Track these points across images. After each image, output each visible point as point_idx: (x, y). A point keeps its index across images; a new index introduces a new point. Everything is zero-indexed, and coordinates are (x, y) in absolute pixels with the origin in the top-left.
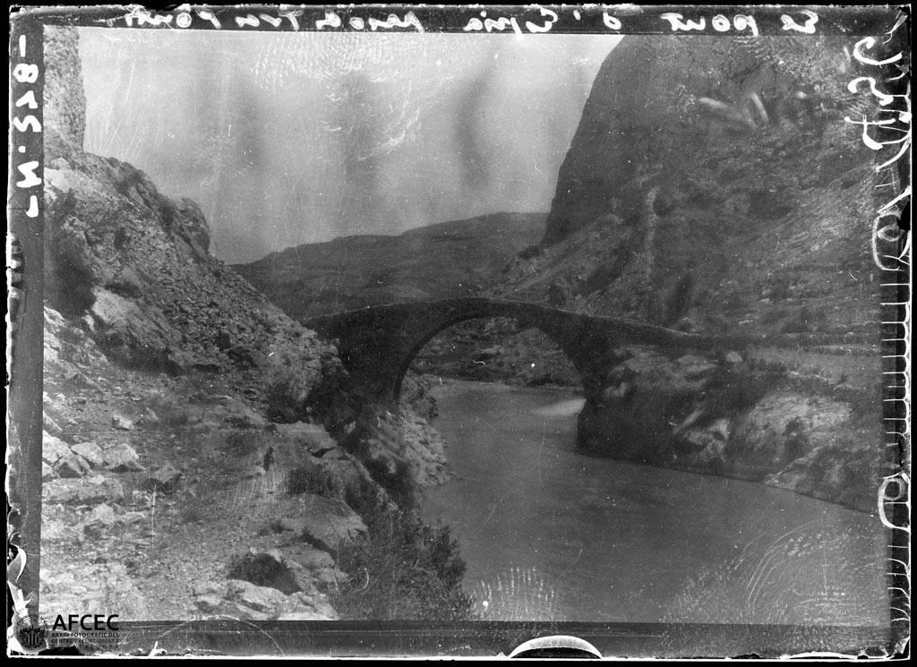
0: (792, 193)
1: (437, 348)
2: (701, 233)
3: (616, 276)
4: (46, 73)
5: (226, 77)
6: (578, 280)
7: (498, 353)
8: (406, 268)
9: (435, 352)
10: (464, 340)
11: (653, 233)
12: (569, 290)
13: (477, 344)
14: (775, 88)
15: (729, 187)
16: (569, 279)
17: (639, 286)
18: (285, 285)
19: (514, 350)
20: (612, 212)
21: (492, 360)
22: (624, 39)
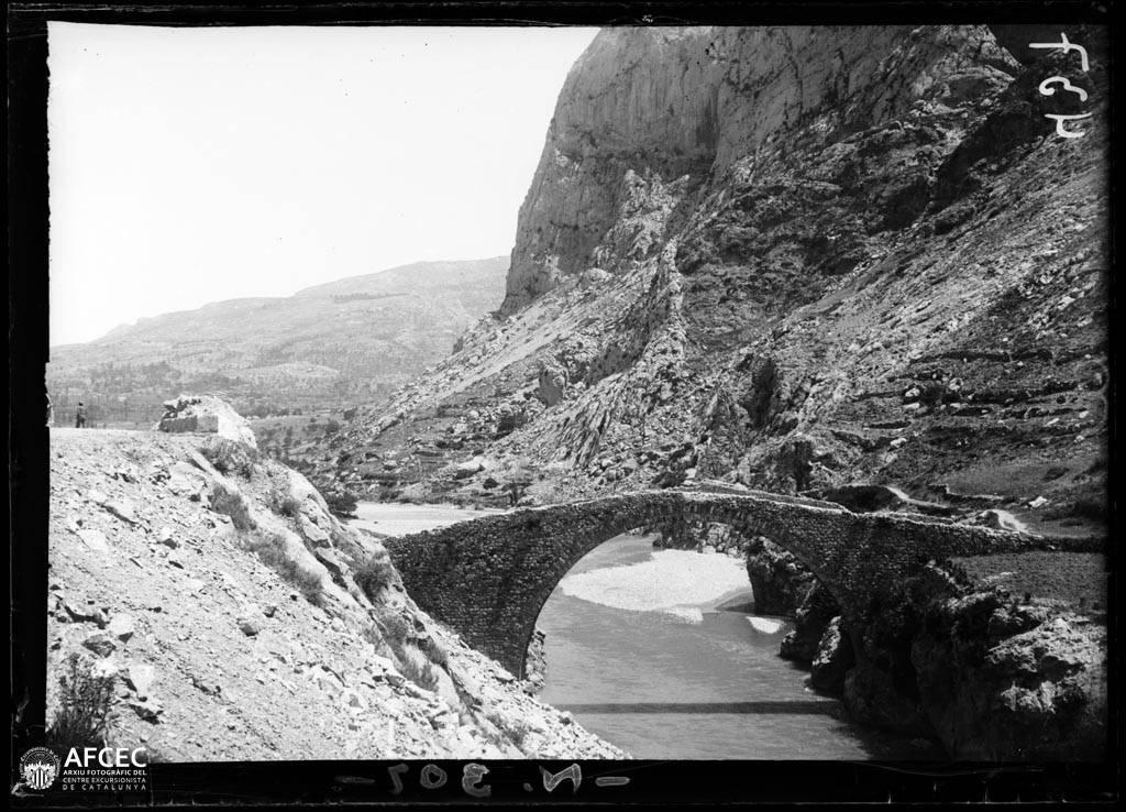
0: (857, 241)
1: (392, 463)
2: (742, 295)
3: (637, 358)
4: (1087, 556)
5: (373, 547)
6: (575, 362)
7: (481, 469)
8: (304, 339)
9: (389, 468)
10: (426, 450)
11: (681, 298)
12: (565, 376)
13: (447, 455)
14: (801, 103)
15: (771, 234)
16: (561, 358)
17: (671, 370)
18: (144, 370)
19: (502, 460)
20: (596, 266)
21: (474, 478)
22: (600, 32)
